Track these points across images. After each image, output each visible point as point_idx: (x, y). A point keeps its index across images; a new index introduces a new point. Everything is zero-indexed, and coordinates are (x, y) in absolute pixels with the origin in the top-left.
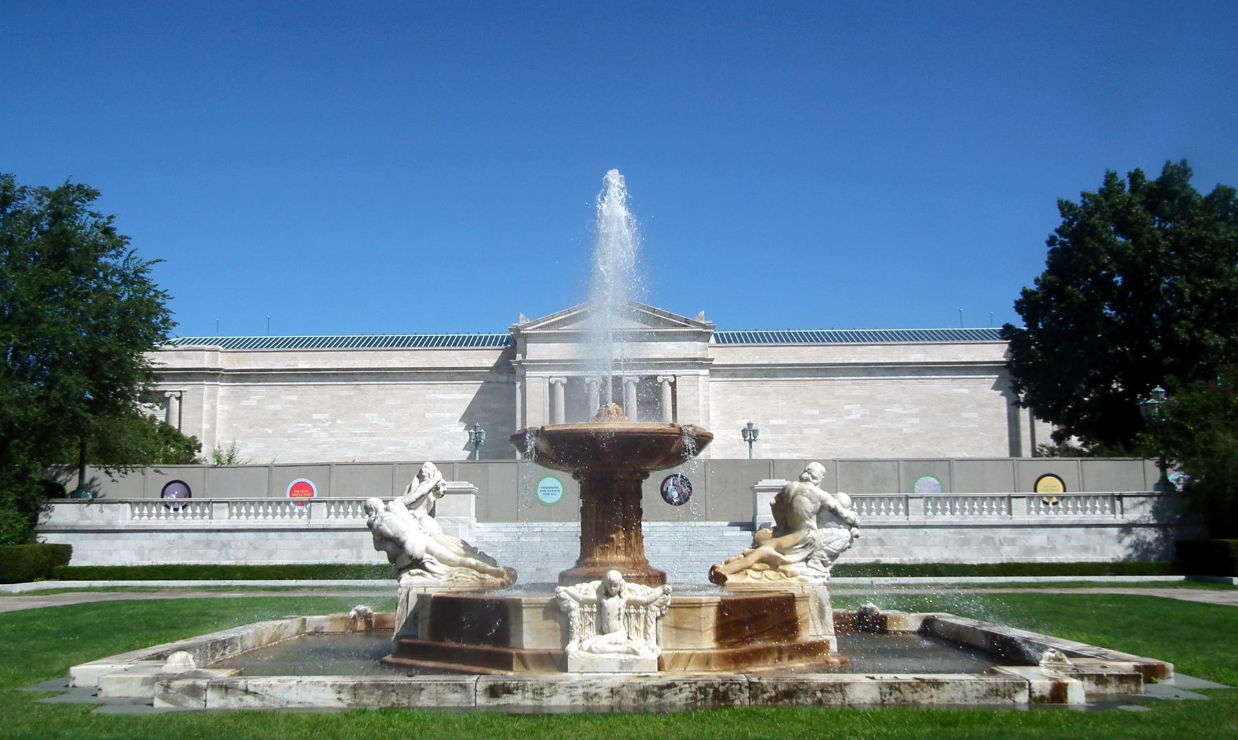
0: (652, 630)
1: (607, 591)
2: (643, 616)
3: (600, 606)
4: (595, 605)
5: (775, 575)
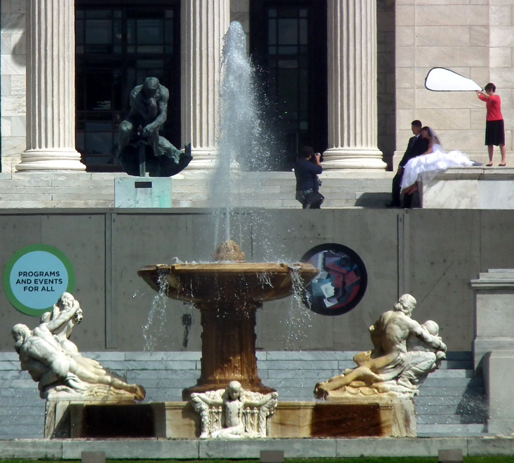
0: (263, 425)
1: (230, 396)
2: (256, 415)
3: (224, 407)
4: (221, 407)
5: (369, 391)
